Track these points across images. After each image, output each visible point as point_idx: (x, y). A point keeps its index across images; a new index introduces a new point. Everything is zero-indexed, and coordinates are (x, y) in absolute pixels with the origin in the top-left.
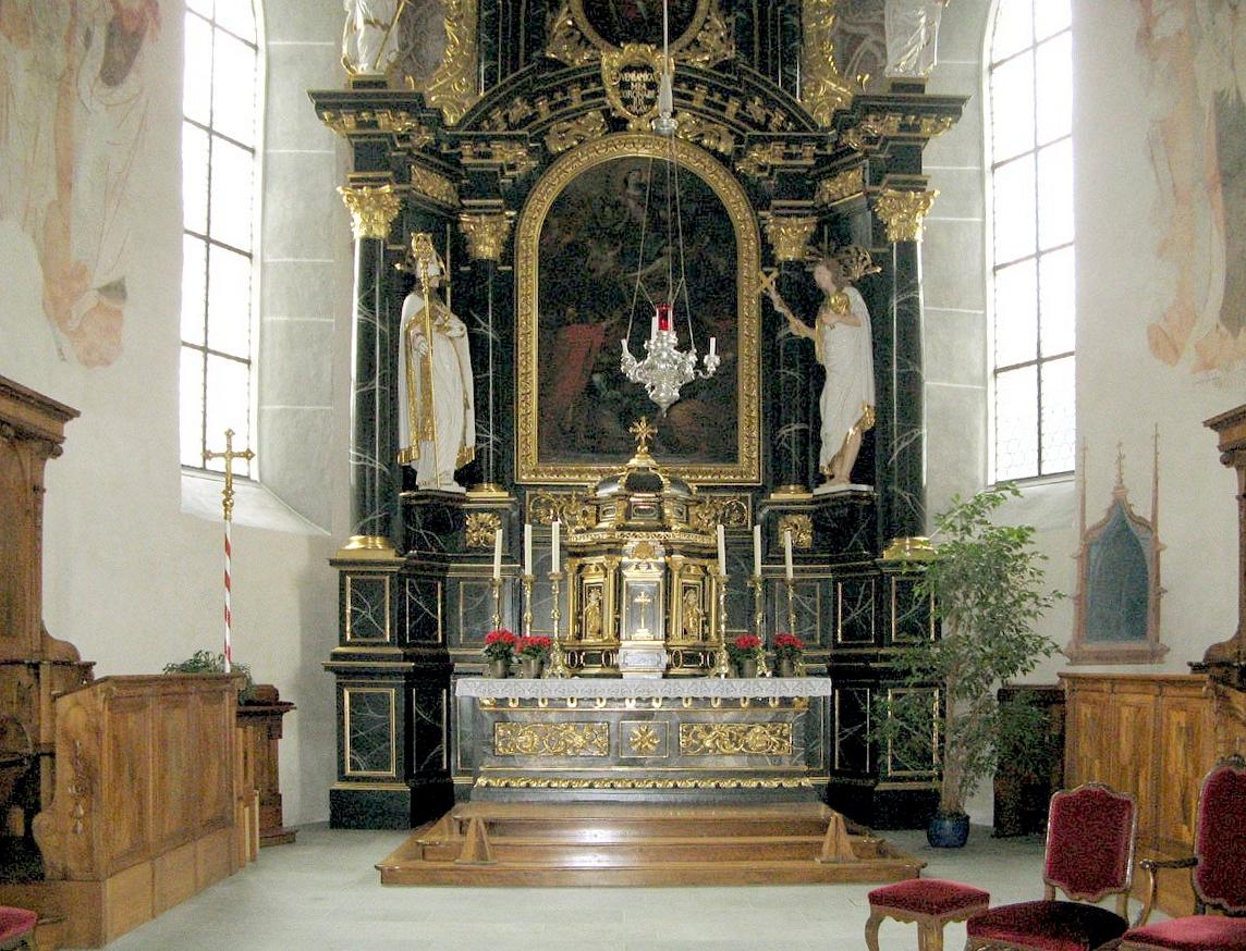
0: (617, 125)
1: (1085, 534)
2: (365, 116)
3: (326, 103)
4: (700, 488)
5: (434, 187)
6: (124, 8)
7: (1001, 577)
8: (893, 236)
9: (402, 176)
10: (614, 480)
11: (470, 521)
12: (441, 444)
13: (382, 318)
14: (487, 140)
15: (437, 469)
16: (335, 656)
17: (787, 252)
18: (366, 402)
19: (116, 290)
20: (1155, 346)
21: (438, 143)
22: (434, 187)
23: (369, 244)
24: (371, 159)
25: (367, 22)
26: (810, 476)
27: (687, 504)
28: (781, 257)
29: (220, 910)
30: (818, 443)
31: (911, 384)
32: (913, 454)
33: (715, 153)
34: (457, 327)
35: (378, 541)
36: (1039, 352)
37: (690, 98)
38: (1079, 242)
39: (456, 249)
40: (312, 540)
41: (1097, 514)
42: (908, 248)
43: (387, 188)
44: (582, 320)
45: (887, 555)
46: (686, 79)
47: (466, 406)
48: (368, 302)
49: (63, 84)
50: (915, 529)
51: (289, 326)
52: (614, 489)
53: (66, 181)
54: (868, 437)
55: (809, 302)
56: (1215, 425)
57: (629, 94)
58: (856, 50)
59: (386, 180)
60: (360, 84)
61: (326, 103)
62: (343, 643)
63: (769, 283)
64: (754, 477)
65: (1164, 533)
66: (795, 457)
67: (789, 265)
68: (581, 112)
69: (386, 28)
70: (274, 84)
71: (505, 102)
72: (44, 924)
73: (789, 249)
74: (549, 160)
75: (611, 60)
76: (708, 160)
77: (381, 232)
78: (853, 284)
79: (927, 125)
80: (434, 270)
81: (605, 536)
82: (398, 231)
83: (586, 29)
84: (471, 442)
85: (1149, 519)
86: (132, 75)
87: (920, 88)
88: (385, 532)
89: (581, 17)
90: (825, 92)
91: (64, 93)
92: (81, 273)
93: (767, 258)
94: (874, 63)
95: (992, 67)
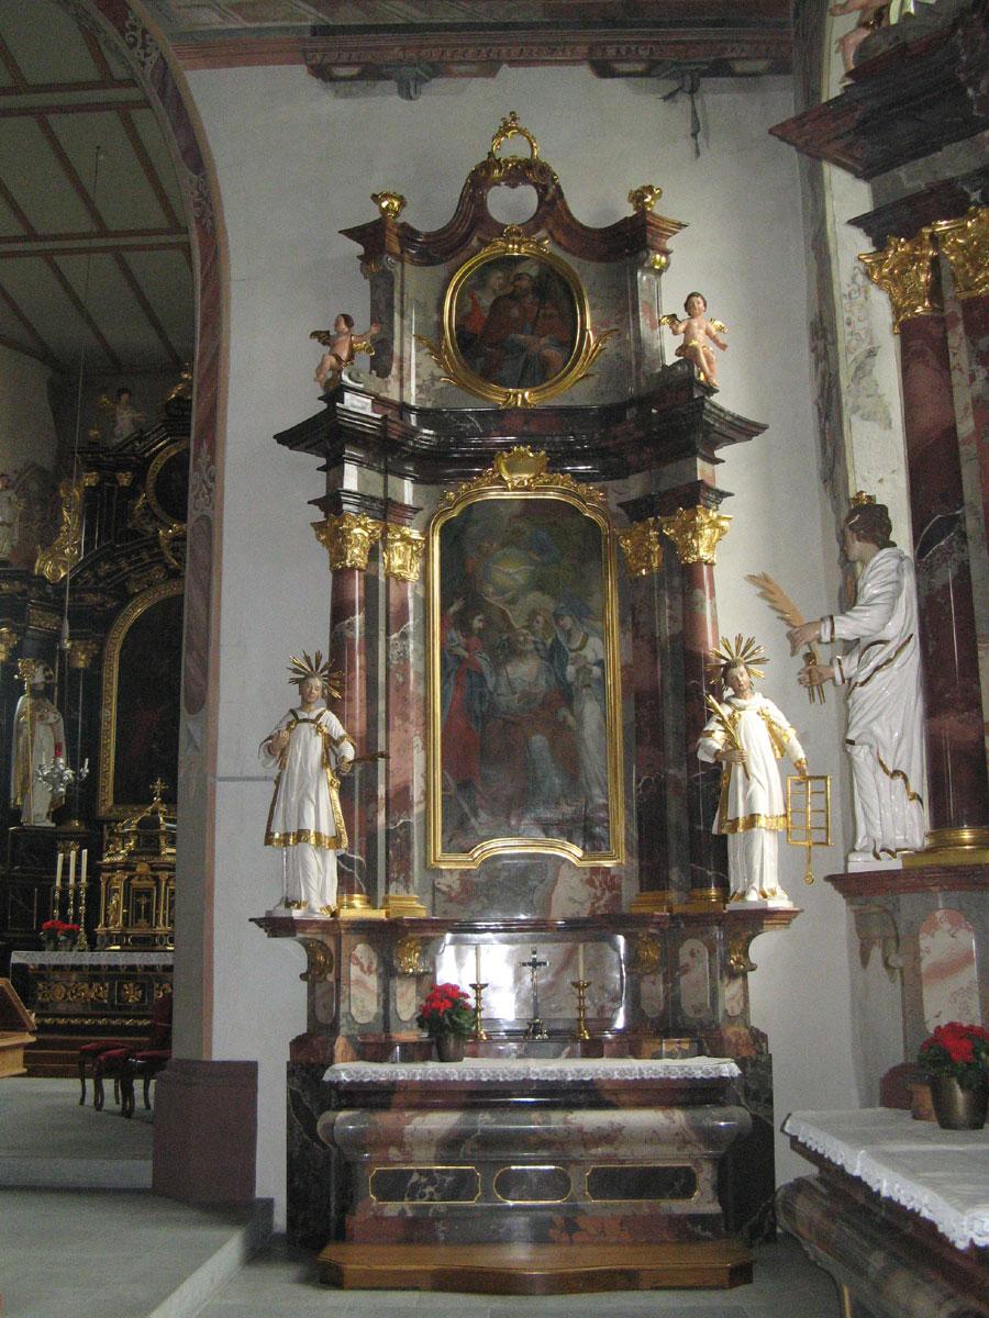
74: (125, 598)
89: (153, 503)
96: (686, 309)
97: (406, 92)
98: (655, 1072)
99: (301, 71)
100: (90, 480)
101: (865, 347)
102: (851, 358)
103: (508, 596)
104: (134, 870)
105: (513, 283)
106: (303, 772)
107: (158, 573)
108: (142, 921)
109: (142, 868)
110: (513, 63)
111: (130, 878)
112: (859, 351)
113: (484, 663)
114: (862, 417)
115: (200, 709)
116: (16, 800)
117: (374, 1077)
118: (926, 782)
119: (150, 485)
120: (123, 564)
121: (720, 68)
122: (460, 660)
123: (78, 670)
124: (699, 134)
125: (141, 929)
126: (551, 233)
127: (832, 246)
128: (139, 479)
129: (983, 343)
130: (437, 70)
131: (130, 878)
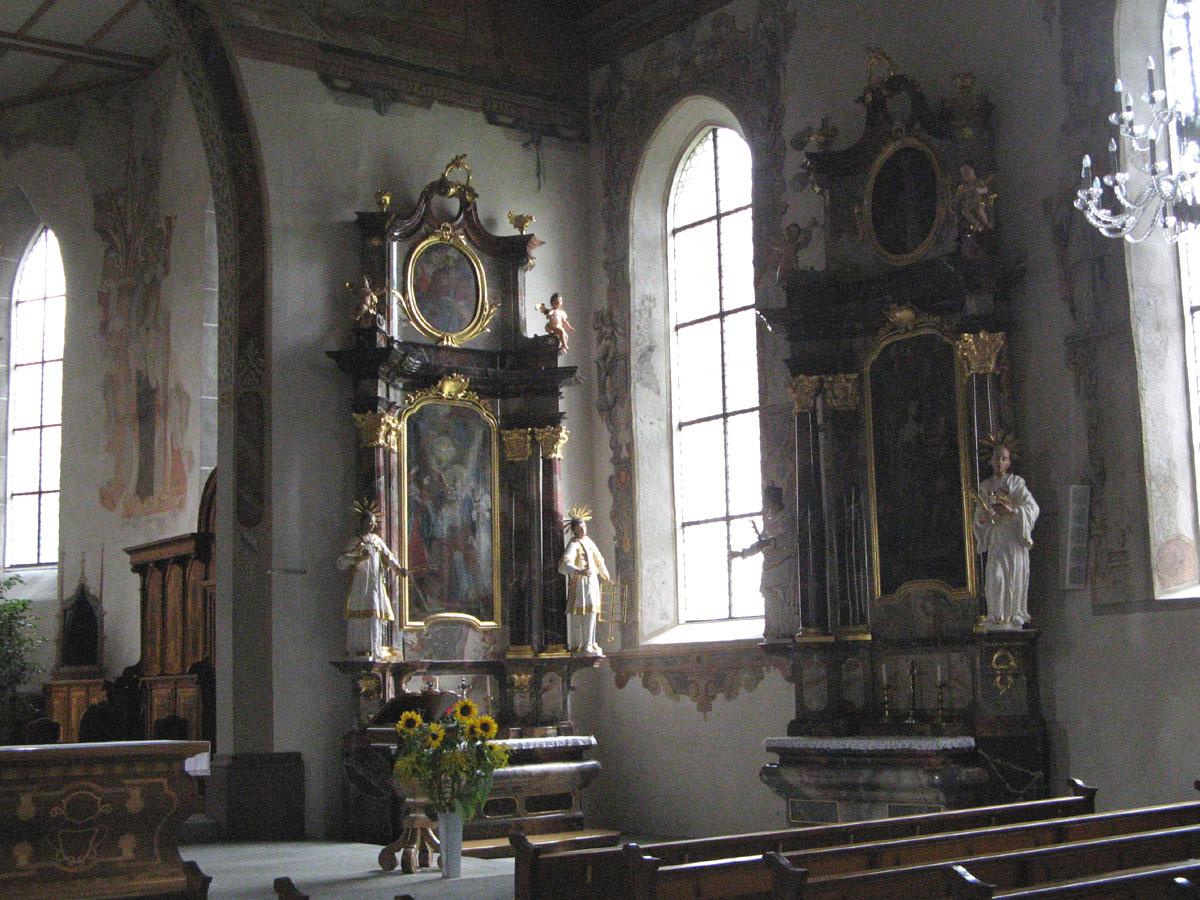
1: (63, 602)
6: (793, 685)
7: (11, 628)
20: (103, 499)
29: (185, 73)
36: (40, 487)
41: (70, 592)
56: (131, 551)
85: (98, 596)
95: (18, 303)
96: (552, 302)
97: (380, 109)
98: (561, 743)
99: (315, 75)
101: (647, 344)
102: (638, 349)
103: (443, 465)
105: (444, 262)
106: (372, 574)
110: (442, 102)
112: (643, 346)
113: (429, 507)
114: (642, 385)
115: (256, 523)
117: (541, 744)
121: (552, 131)
122: (417, 503)
124: (541, 175)
126: (465, 230)
127: (631, 278)
130: (396, 96)
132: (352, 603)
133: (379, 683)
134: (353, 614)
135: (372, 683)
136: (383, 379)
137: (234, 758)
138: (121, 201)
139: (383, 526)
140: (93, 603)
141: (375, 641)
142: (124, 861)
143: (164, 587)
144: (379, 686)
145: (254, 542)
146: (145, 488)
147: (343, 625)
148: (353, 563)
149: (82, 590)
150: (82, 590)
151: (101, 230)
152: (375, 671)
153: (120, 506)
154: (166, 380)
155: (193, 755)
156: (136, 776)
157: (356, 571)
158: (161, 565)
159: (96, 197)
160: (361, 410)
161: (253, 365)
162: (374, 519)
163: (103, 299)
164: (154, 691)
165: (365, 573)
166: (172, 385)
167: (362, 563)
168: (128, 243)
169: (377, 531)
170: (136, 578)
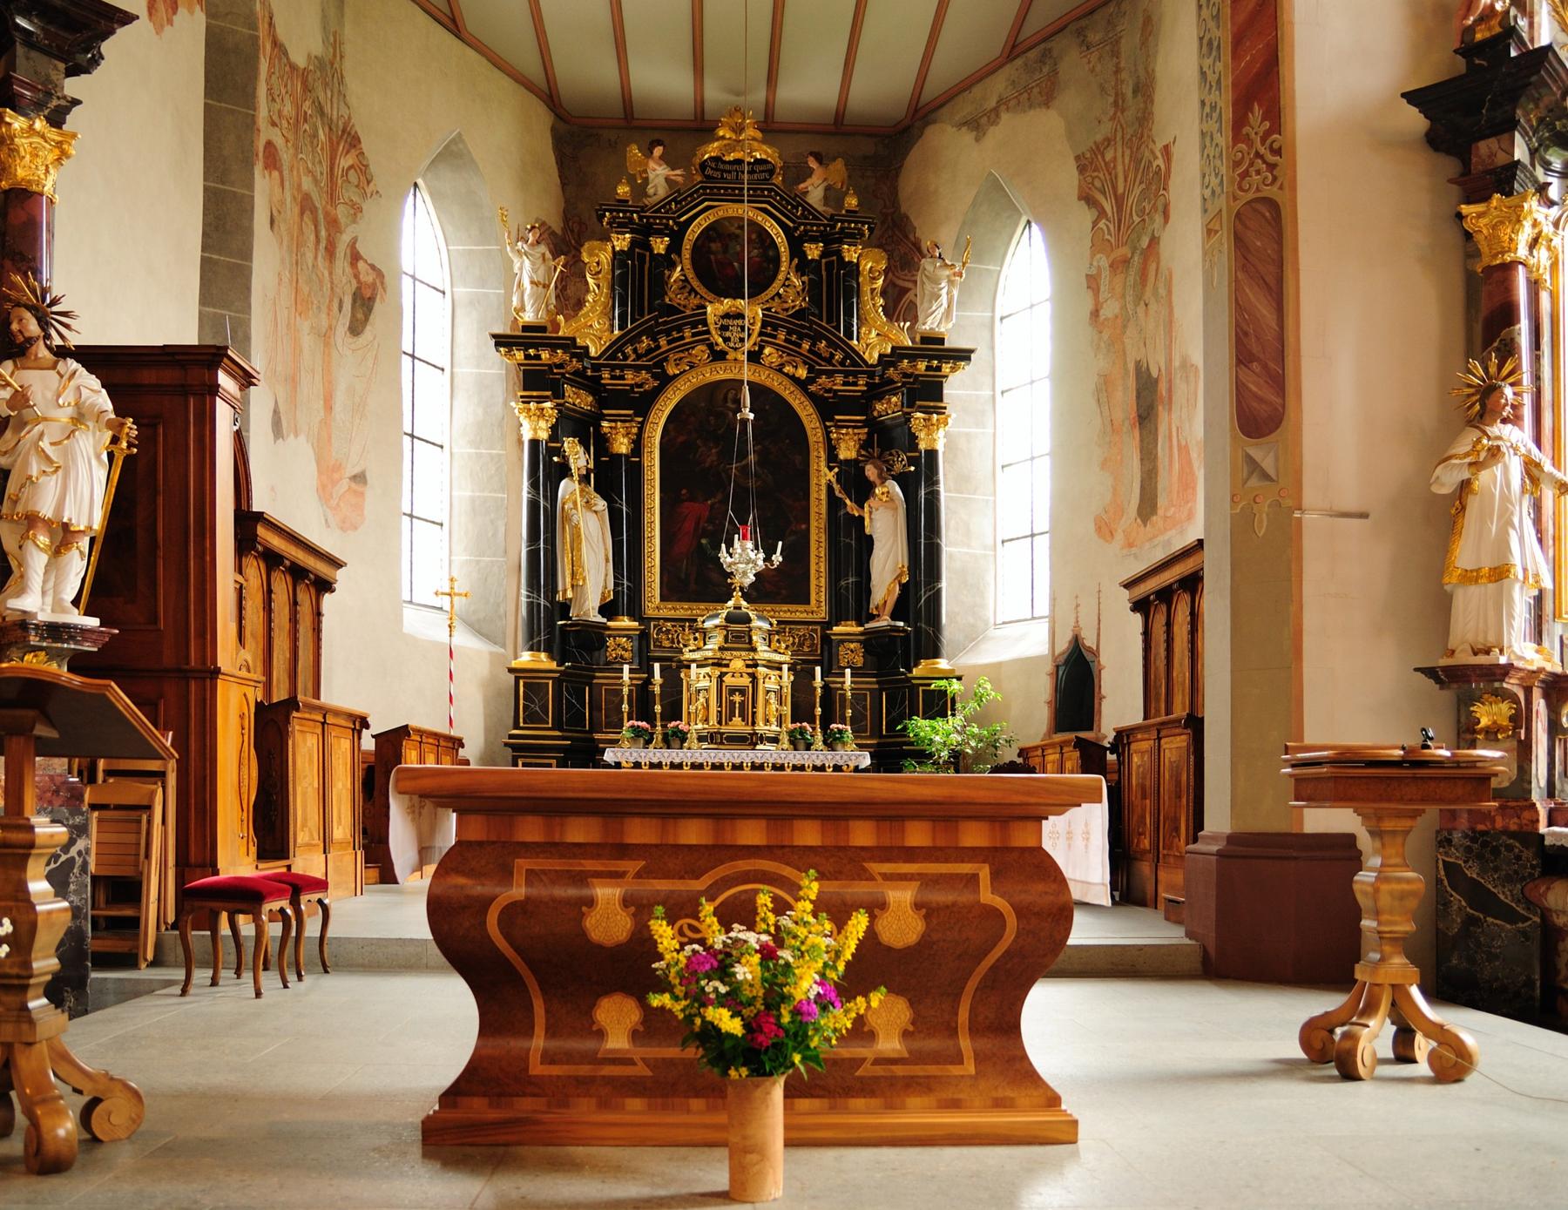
0: (718, 356)
1: (1055, 659)
2: (532, 352)
3: (501, 341)
4: (779, 623)
5: (581, 400)
8: (922, 446)
9: (558, 394)
10: (717, 616)
11: (610, 642)
12: (590, 578)
13: (545, 497)
14: (622, 368)
15: (589, 608)
16: (511, 737)
17: (847, 452)
18: (533, 556)
19: (360, 478)
20: (1099, 530)
21: (585, 368)
22: (581, 400)
23: (534, 443)
24: (536, 382)
25: (532, 282)
26: (863, 614)
27: (770, 633)
28: (841, 457)
30: (869, 592)
31: (934, 552)
32: (935, 599)
33: (793, 378)
34: (601, 504)
35: (543, 656)
37: (775, 337)
38: (1052, 454)
39: (599, 445)
40: (491, 653)
41: (1063, 645)
42: (932, 455)
43: (548, 405)
44: (692, 499)
45: (915, 672)
46: (770, 324)
47: (607, 560)
48: (534, 485)
49: (326, 337)
50: (936, 653)
51: (473, 500)
52: (717, 621)
53: (329, 406)
54: (904, 588)
55: (863, 491)
57: (728, 334)
58: (899, 303)
59: (546, 399)
60: (526, 328)
61: (501, 341)
62: (517, 726)
63: (831, 476)
64: (822, 614)
65: (1103, 659)
66: (851, 597)
67: (847, 461)
68: (693, 345)
69: (546, 286)
70: (457, 321)
71: (635, 340)
72: (1256, 210)
73: (847, 452)
74: (665, 380)
75: (714, 310)
76: (786, 381)
77: (543, 435)
78: (894, 478)
79: (946, 368)
80: (582, 463)
81: (710, 654)
82: (555, 435)
83: (695, 283)
84: (611, 586)
86: (368, 328)
87: (942, 341)
88: (548, 650)
89: (691, 275)
90: (874, 339)
91: (327, 344)
92: (338, 467)
93: (832, 456)
94: (912, 314)
100: (622, 242)
104: (727, 666)
106: (1505, 498)
107: (701, 352)
108: (737, 719)
109: (738, 664)
111: (722, 675)
116: (565, 591)
118: (911, 1133)
119: (686, 254)
120: (663, 342)
123: (620, 455)
125: (737, 726)
128: (675, 247)
129: (7, 1032)
131: (722, 675)
132: (1465, 555)
133: (1519, 710)
134: (1471, 577)
135: (1504, 710)
136: (1524, 134)
137: (1232, 839)
138: (1109, 156)
139: (1527, 412)
140: (1089, 657)
141: (1511, 626)
142: (878, 1061)
143: (1169, 625)
144: (1519, 710)
145: (1268, 464)
146: (1148, 506)
147: (1442, 605)
148: (1466, 475)
149: (1076, 642)
150: (1076, 642)
151: (1087, 199)
152: (1512, 684)
153: (1119, 536)
154: (1169, 360)
155: (1061, 807)
156: (910, 854)
157: (1472, 492)
158: (1166, 595)
159: (1077, 158)
160: (1477, 195)
161: (1262, 151)
162: (1508, 391)
163: (1093, 282)
164: (1133, 746)
165: (1493, 495)
166: (1176, 363)
167: (1484, 475)
168: (1119, 201)
169: (1516, 419)
170: (1137, 619)
